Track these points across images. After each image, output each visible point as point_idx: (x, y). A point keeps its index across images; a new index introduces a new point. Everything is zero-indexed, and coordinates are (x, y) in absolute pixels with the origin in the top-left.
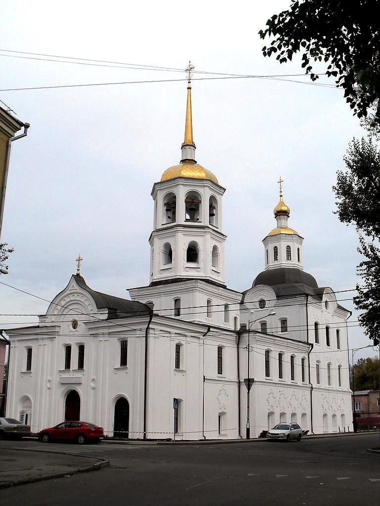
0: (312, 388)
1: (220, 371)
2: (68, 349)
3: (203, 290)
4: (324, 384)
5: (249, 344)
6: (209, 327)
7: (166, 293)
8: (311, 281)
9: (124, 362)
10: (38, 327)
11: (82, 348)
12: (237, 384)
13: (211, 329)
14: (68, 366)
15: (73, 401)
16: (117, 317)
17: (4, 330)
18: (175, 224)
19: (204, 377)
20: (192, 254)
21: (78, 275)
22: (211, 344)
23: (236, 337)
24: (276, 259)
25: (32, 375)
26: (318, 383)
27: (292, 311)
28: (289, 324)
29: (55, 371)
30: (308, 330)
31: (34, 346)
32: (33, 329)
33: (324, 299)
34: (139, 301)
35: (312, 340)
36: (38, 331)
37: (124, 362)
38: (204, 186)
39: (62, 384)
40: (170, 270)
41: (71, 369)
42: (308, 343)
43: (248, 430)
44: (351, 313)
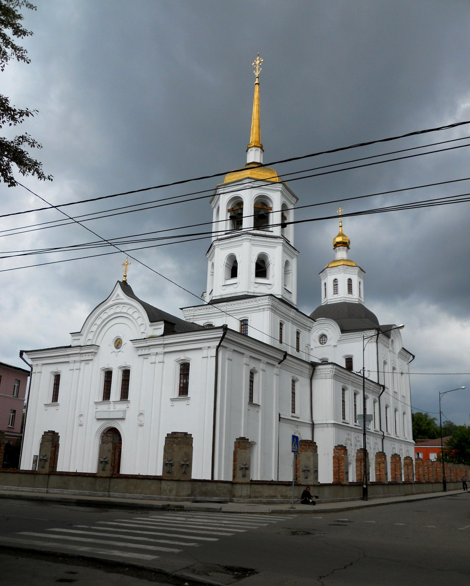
0: (383, 436)
2: (108, 374)
5: (364, 368)
9: (184, 390)
10: (70, 347)
11: (126, 373)
13: (288, 357)
14: (107, 395)
15: (112, 439)
16: (174, 332)
17: (26, 352)
19: (280, 415)
20: (261, 269)
21: (125, 282)
23: (309, 369)
25: (59, 407)
30: (378, 372)
31: (64, 371)
32: (64, 349)
34: (194, 322)
36: (69, 351)
37: (184, 390)
39: (98, 419)
40: (235, 286)
44: (414, 357)
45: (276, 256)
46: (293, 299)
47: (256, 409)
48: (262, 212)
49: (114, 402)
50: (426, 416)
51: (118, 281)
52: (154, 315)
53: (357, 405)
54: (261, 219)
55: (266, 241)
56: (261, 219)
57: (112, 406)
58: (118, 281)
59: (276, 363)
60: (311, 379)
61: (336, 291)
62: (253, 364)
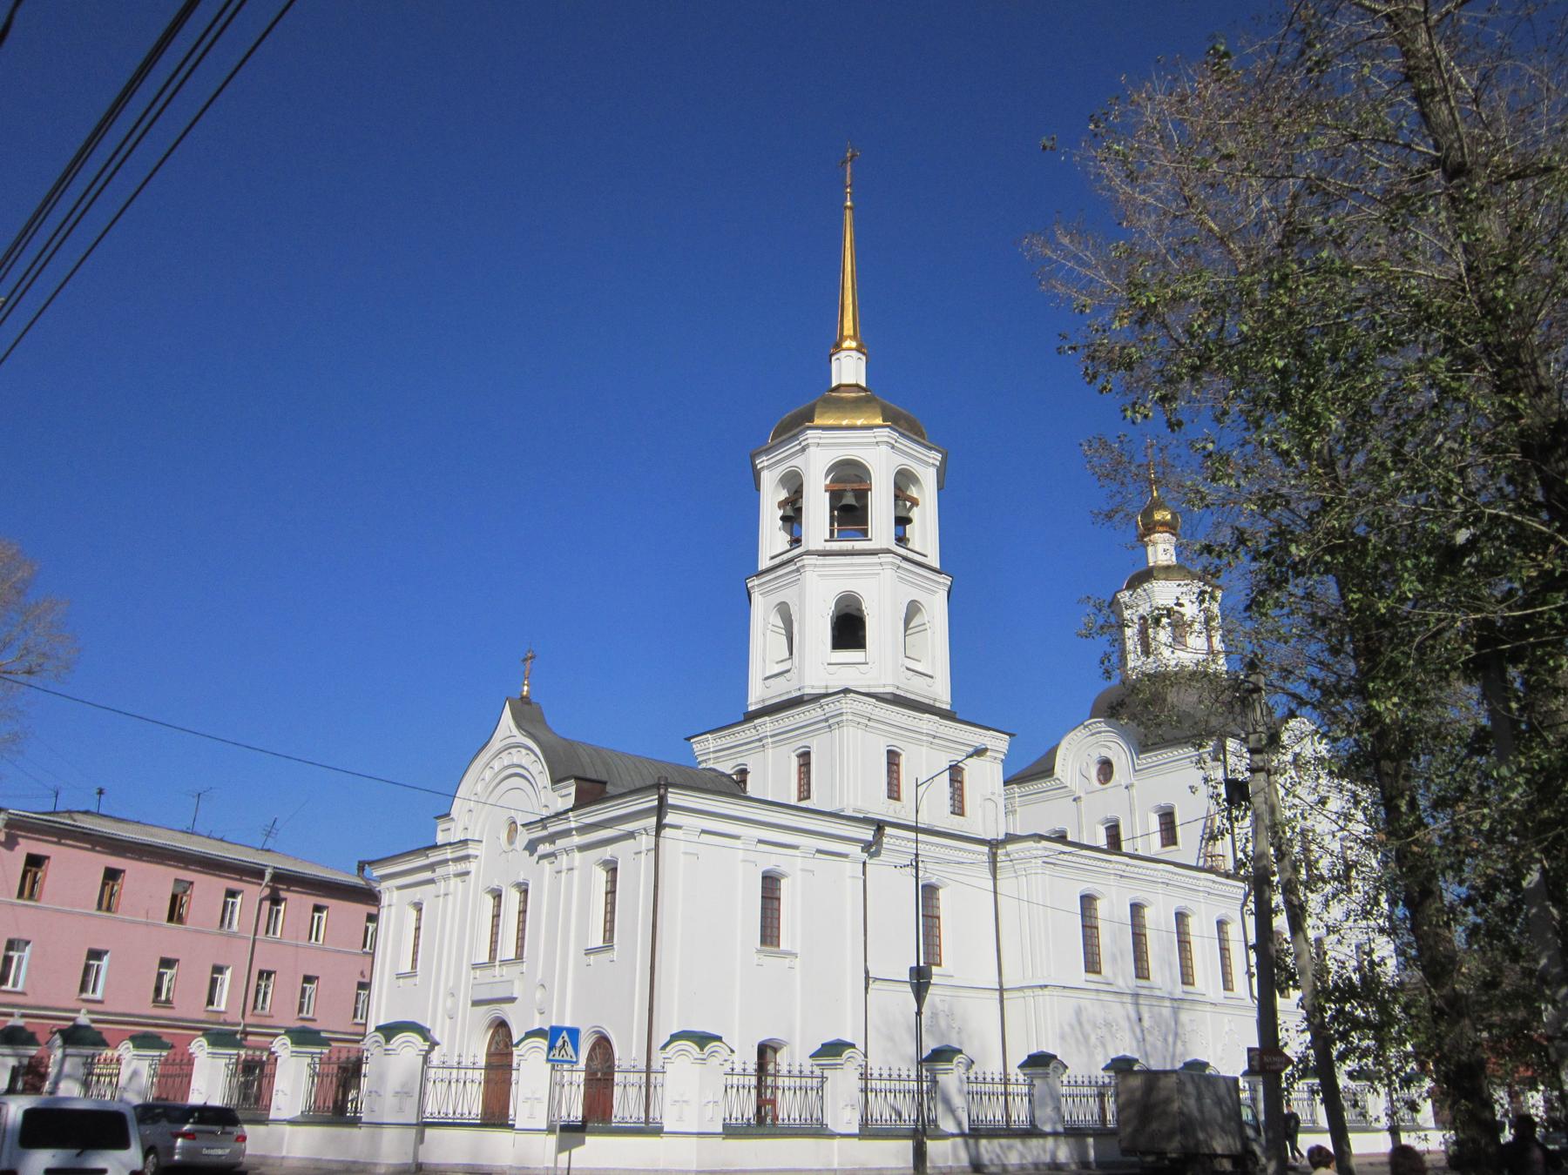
12: (997, 994)
20: (849, 629)
45: (882, 591)
48: (849, 499)
54: (850, 513)
56: (850, 513)
59: (855, 850)
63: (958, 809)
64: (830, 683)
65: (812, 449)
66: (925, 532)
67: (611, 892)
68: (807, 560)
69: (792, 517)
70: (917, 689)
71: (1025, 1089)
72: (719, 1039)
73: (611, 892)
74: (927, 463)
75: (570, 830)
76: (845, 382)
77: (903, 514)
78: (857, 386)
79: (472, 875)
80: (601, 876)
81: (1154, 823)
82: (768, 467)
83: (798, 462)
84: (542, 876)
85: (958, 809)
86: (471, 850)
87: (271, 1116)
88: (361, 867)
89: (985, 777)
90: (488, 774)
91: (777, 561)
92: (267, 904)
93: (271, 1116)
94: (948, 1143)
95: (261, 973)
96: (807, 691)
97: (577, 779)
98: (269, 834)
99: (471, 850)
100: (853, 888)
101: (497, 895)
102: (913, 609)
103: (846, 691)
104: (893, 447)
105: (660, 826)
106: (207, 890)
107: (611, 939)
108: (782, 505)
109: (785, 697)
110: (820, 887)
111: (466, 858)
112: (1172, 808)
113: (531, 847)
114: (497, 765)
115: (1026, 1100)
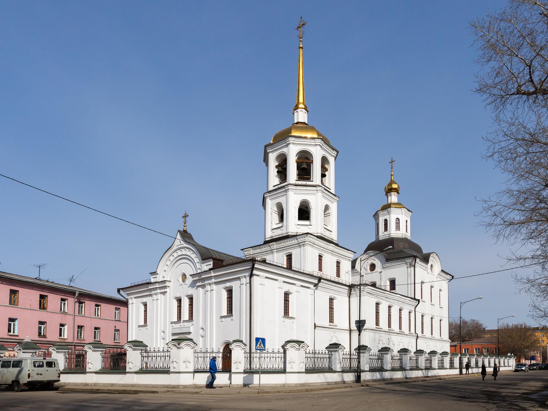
0: (417, 337)
1: (331, 320)
3: (313, 245)
4: (427, 332)
6: (320, 279)
7: (279, 250)
8: (418, 249)
12: (348, 332)
17: (122, 289)
18: (286, 183)
20: (304, 213)
21: (185, 231)
22: (323, 295)
24: (386, 229)
26: (422, 333)
27: (399, 271)
28: (397, 283)
29: (168, 323)
30: (415, 283)
33: (430, 263)
35: (418, 297)
38: (316, 145)
41: (182, 320)
42: (414, 299)
43: (258, 276)
45: (317, 201)
46: (334, 236)
47: (292, 320)
48: (305, 166)
49: (184, 321)
50: (481, 325)
51: (179, 231)
52: (205, 255)
53: (392, 314)
54: (304, 172)
55: (306, 190)
56: (304, 172)
57: (182, 324)
58: (179, 231)
59: (312, 286)
60: (349, 297)
61: (398, 227)
62: (287, 287)
63: (338, 275)
64: (298, 232)
65: (291, 145)
66: (330, 181)
67: (146, 311)
68: (290, 187)
69: (282, 172)
70: (327, 235)
71: (356, 357)
72: (303, 342)
73: (146, 311)
74: (331, 155)
75: (212, 276)
76: (300, 121)
77: (323, 173)
78: (304, 123)
79: (168, 293)
80: (142, 308)
81: (388, 283)
82: (272, 152)
83: (285, 150)
84: (199, 294)
85: (338, 275)
86: (167, 284)
87: (127, 371)
88: (119, 291)
89: (346, 266)
90: (172, 258)
91: (276, 187)
92: (77, 304)
93: (127, 371)
94: (336, 374)
95: (78, 327)
96: (290, 234)
97: (213, 259)
98: (71, 281)
99: (167, 284)
100: (310, 299)
101: (179, 301)
102: (327, 208)
103: (308, 233)
104: (321, 147)
105: (251, 275)
106: (53, 300)
107: (146, 323)
108: (277, 167)
109: (281, 236)
110: (301, 296)
111: (165, 287)
112: (395, 279)
113: (194, 282)
114: (175, 255)
115: (349, 360)
